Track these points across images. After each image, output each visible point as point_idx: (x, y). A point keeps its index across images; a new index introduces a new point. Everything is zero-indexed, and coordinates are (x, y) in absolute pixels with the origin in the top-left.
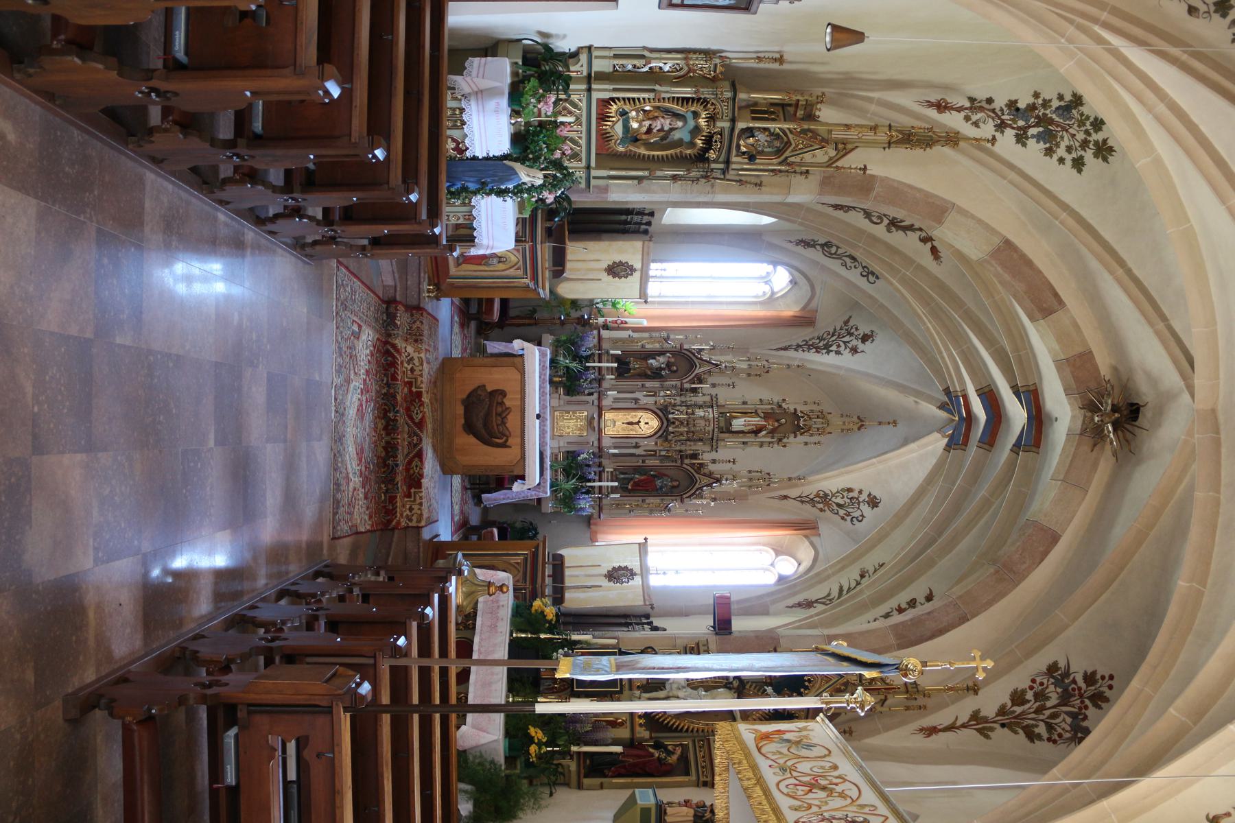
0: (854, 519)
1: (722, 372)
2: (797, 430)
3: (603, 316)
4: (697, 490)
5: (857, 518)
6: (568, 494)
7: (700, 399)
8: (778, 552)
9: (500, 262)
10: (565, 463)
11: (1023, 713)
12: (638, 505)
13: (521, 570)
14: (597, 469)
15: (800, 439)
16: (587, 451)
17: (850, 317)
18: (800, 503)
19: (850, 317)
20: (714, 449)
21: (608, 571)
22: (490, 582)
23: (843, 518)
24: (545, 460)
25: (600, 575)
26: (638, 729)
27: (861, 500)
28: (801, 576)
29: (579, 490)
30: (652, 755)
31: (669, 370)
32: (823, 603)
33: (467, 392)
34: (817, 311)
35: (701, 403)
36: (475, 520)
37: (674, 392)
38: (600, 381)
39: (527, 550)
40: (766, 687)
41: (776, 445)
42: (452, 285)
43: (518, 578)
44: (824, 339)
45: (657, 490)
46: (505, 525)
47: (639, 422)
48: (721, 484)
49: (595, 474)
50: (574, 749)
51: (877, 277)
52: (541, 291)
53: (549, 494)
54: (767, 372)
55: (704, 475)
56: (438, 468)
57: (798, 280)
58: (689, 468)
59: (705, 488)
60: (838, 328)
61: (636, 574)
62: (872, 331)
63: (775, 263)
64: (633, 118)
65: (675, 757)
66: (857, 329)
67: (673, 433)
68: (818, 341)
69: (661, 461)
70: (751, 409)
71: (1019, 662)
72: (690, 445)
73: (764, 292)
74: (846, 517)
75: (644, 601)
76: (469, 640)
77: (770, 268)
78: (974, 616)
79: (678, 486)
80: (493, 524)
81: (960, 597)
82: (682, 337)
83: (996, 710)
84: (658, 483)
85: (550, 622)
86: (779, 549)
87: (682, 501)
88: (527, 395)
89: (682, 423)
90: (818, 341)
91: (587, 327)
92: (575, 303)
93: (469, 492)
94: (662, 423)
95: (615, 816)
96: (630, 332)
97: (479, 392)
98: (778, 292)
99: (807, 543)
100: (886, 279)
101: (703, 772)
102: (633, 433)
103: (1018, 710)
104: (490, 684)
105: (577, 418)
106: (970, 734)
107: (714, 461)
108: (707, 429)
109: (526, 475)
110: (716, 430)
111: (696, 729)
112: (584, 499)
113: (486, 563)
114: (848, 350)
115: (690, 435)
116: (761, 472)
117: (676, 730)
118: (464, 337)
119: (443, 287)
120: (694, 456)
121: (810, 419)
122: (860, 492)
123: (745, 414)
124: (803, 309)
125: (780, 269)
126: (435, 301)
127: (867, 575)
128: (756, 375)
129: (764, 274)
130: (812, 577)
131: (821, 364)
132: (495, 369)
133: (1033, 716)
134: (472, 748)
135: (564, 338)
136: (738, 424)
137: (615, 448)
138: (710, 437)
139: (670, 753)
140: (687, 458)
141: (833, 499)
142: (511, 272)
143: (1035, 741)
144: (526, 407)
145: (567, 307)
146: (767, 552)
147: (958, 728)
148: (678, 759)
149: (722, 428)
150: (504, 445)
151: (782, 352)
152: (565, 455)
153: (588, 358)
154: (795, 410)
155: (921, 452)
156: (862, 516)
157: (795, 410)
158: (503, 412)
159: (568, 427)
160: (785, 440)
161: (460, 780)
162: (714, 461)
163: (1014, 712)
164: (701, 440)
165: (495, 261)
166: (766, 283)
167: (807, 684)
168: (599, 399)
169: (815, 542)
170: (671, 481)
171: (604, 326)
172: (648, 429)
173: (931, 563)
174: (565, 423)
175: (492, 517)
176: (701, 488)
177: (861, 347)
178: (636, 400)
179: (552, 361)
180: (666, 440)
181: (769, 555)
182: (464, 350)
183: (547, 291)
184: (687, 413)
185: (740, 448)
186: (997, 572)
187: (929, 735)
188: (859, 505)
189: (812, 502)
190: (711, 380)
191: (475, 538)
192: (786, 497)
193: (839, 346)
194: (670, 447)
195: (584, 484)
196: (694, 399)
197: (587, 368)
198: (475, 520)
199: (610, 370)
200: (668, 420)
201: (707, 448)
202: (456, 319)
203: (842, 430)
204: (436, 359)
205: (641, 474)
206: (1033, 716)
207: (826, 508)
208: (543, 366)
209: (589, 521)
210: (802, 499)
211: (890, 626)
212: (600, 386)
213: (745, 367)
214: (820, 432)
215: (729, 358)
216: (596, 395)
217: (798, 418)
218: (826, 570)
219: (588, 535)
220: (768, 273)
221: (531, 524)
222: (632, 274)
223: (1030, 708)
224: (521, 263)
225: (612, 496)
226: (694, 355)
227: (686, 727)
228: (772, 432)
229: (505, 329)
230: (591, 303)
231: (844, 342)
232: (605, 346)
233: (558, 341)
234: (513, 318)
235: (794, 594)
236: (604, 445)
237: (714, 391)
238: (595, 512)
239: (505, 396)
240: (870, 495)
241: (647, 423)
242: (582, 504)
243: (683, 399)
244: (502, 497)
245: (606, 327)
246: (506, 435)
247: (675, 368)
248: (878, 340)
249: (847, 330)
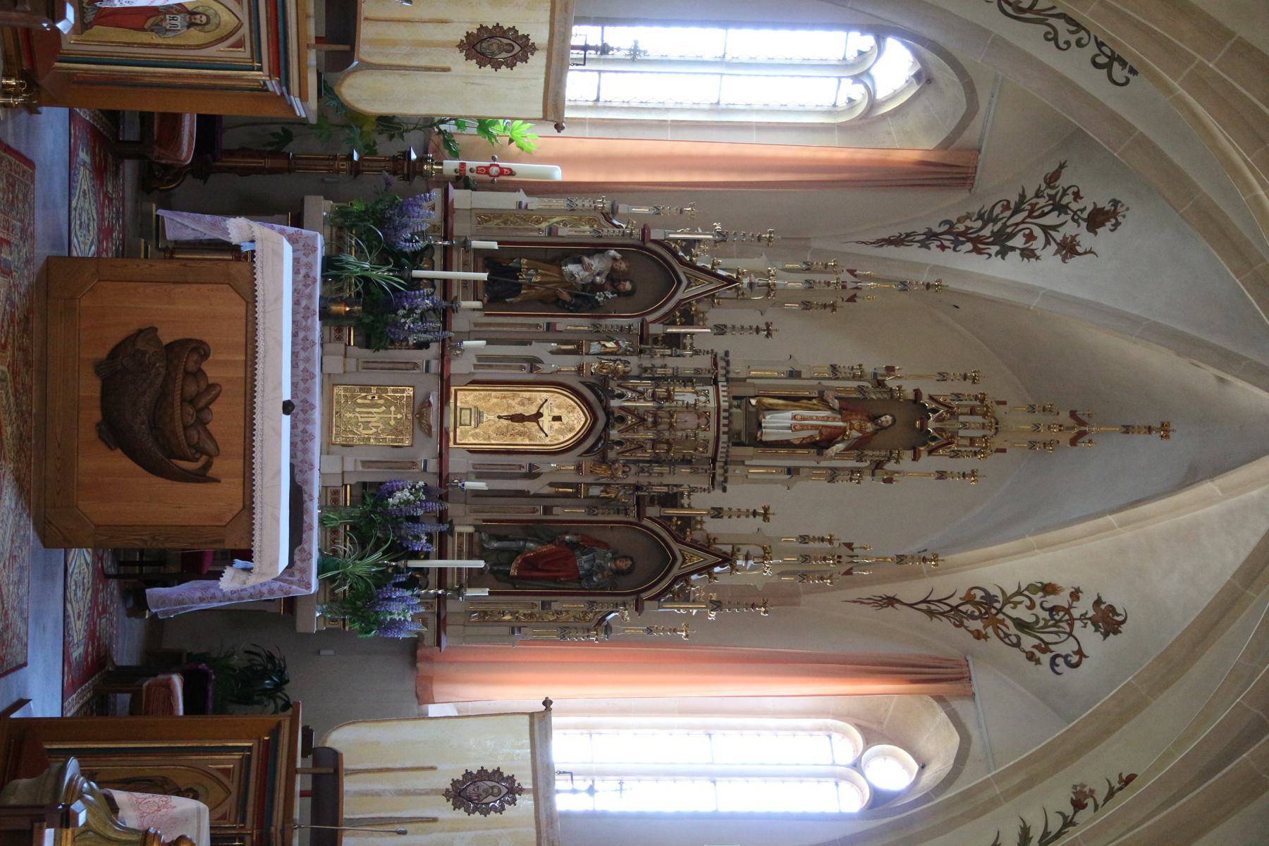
0: (1060, 661)
1: (740, 296)
2: (921, 442)
3: (455, 155)
4: (675, 581)
5: (1066, 657)
6: (362, 586)
7: (686, 363)
8: (872, 735)
9: (191, 25)
10: (357, 512)
12: (531, 615)
13: (233, 787)
14: (435, 528)
15: (929, 463)
16: (410, 483)
17: (1062, 166)
18: (925, 617)
19: (1062, 166)
20: (718, 483)
21: (455, 783)
22: (146, 833)
23: (1030, 657)
24: (308, 504)
25: (434, 792)
27: (1076, 613)
28: (926, 798)
29: (390, 577)
31: (616, 291)
33: (110, 347)
34: (979, 151)
35: (689, 372)
36: (126, 652)
37: (623, 344)
38: (445, 314)
39: (249, 738)
41: (867, 478)
42: (70, 77)
43: (220, 811)
44: (995, 221)
45: (580, 579)
46: (203, 666)
47: (539, 415)
48: (734, 568)
49: (430, 541)
51: (1133, 71)
52: (296, 102)
53: (314, 587)
54: (852, 299)
55: (694, 545)
56: (31, 532)
57: (936, 73)
58: (657, 528)
59: (694, 577)
60: (1030, 194)
61: (521, 791)
62: (1115, 203)
63: (880, 32)
66: (1077, 196)
67: (619, 443)
68: (979, 223)
69: (591, 509)
70: (811, 388)
72: (661, 474)
73: (851, 100)
74: (1038, 654)
77: (866, 41)
79: (630, 571)
80: (172, 661)
82: (645, 210)
84: (583, 562)
86: (874, 727)
87: (639, 608)
88: (260, 355)
89: (642, 420)
90: (979, 223)
91: (417, 179)
92: (388, 124)
93: (113, 584)
94: (595, 419)
96: (521, 196)
97: (140, 345)
98: (884, 103)
99: (942, 716)
100: (1156, 79)
102: (523, 442)
105: (388, 404)
107: (718, 513)
108: (701, 435)
109: (256, 549)
110: (724, 438)
112: (402, 599)
113: (148, 771)
114: (1053, 247)
115: (661, 449)
116: (830, 541)
118: (105, 200)
119: (44, 82)
120: (671, 499)
121: (953, 415)
122: (1075, 595)
123: (794, 400)
124: (946, 145)
125: (893, 44)
126: (24, 115)
127: (1090, 801)
128: (825, 306)
129: (852, 55)
130: (950, 804)
131: (988, 281)
132: (183, 288)
135: (358, 207)
136: (778, 424)
137: (480, 477)
138: (710, 454)
140: (652, 503)
141: (1008, 609)
142: (220, 51)
144: (259, 383)
145: (366, 128)
146: (845, 733)
149: (739, 434)
150: (201, 476)
151: (890, 251)
152: (358, 492)
153: (417, 259)
154: (917, 393)
155: (1233, 501)
156: (1080, 652)
157: (917, 393)
158: (199, 395)
159: (366, 425)
160: (890, 466)
162: (718, 513)
164: (686, 461)
165: (180, 20)
166: (857, 79)
168: (444, 358)
169: (961, 713)
170: (614, 559)
171: (458, 178)
172: (560, 431)
174: (358, 415)
175: (170, 643)
176: (685, 577)
177: (1086, 239)
178: (533, 362)
179: (328, 263)
180: (603, 459)
181: (847, 744)
182: (105, 233)
183: (313, 103)
184: (654, 397)
185: (783, 482)
188: (1071, 626)
189: (956, 614)
190: (716, 316)
191: (124, 699)
192: (891, 601)
193: (1030, 237)
194: (613, 476)
195: (401, 564)
196: (672, 362)
197: (416, 283)
198: (126, 652)
199: (472, 289)
200: (608, 412)
201: (702, 481)
202: (83, 156)
203: (1032, 445)
204: (28, 261)
205: (540, 541)
207: (990, 630)
208: (307, 276)
209: (412, 651)
210: (930, 608)
212: (446, 326)
213: (799, 285)
214: (979, 447)
215: (759, 263)
216: (435, 348)
217: (924, 413)
218: (986, 785)
219: (410, 685)
220: (861, 53)
221: (271, 657)
222: (525, 59)
224: (245, 30)
225: (471, 592)
226: (675, 254)
228: (859, 446)
229: (212, 178)
230: (428, 123)
231: (1045, 229)
232: (460, 227)
233: (343, 213)
234: (231, 153)
236: (451, 470)
237: (720, 344)
238: (429, 632)
239: (206, 355)
240: (1098, 602)
241: (557, 418)
242: (397, 612)
243: (646, 363)
244: (198, 594)
245: (462, 181)
246: (205, 451)
247: (628, 286)
248: (1129, 223)
249: (1052, 197)
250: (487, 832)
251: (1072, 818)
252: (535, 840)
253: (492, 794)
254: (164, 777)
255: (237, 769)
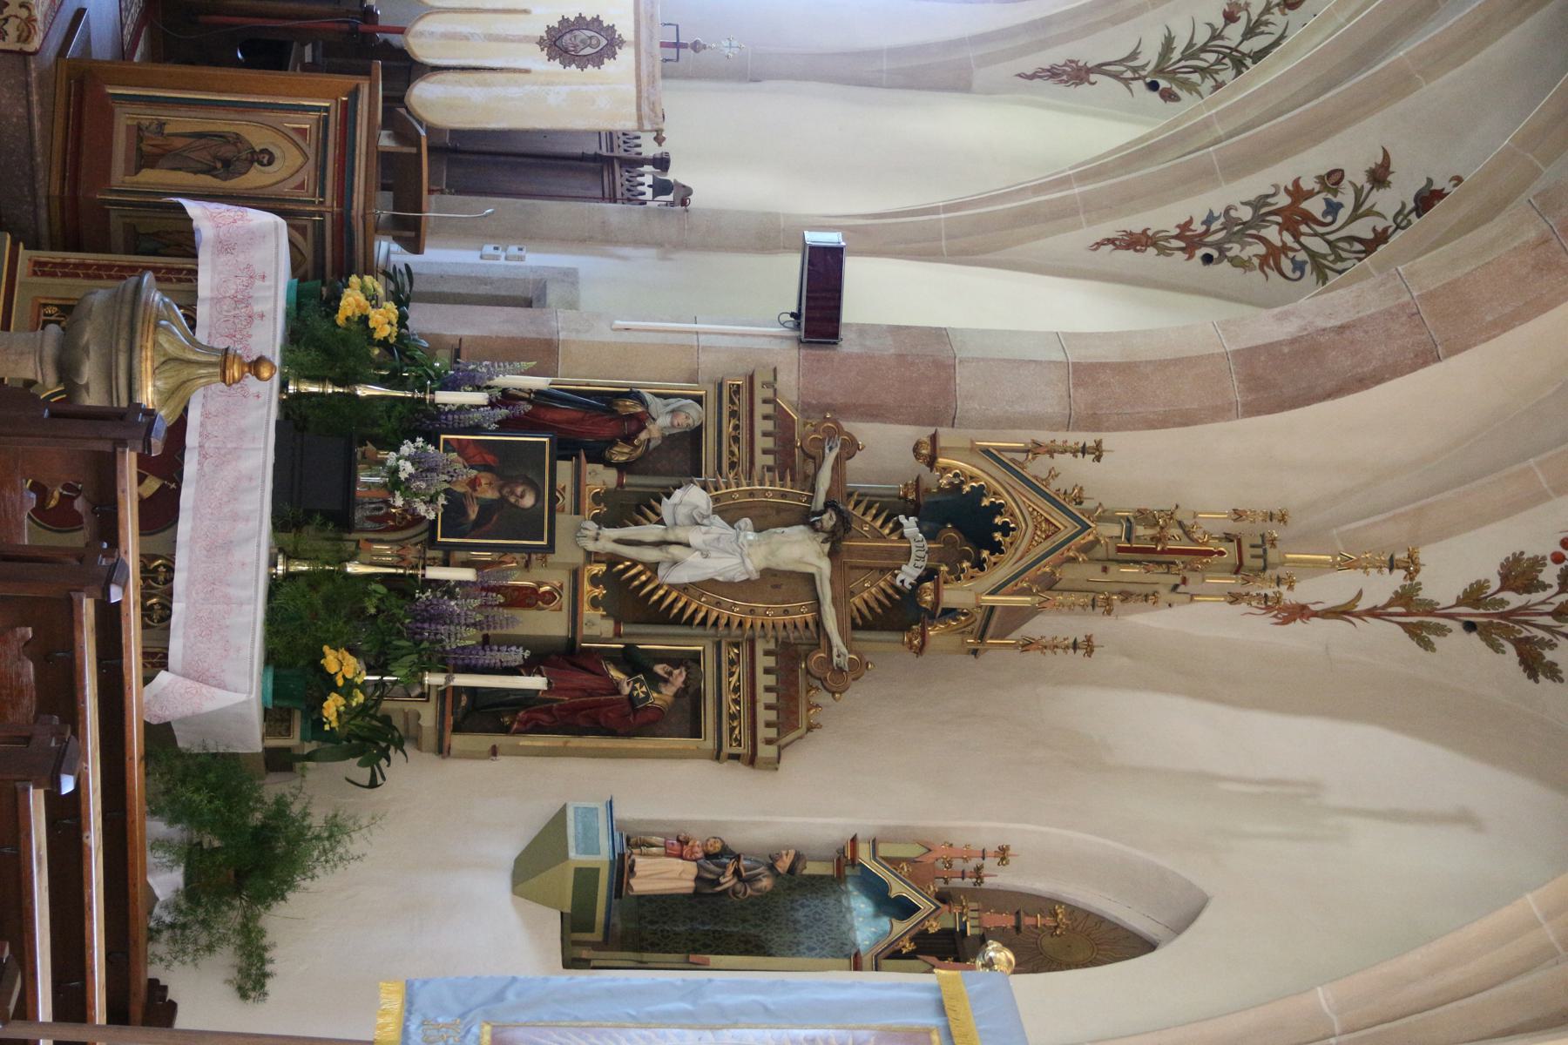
11: (1524, 609)
25: (525, 39)
26: (587, 611)
30: (615, 688)
32: (1116, 76)
39: (325, 97)
40: (902, 518)
50: (434, 679)
64: (517, 501)
65: (668, 691)
71: (1540, 498)
75: (640, 118)
78: (1452, 352)
81: (1429, 297)
83: (1458, 590)
85: (384, 343)
95: (518, 861)
101: (732, 730)
103: (1514, 600)
104: (228, 546)
106: (1389, 633)
111: (723, 621)
117: (677, 621)
127: (1243, 15)
133: (1548, 621)
134: (184, 720)
139: (655, 681)
143: (1541, 677)
147: (1359, 615)
148: (676, 695)
161: (155, 812)
163: (1503, 602)
167: (998, 536)
173: (1401, 84)
186: (1544, 241)
187: (1286, 622)
206: (1548, 621)
211: (1237, 353)
223: (1543, 602)
227: (701, 615)
235: (1044, 45)
250: (584, 88)
251: (1222, 31)
252: (634, 99)
253: (590, 46)
255: (314, 129)
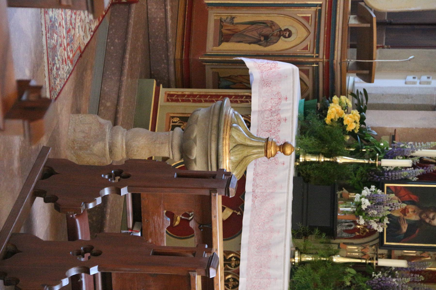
13: (312, 29)
76: (248, 80)
104: (268, 246)
254: (271, 21)
